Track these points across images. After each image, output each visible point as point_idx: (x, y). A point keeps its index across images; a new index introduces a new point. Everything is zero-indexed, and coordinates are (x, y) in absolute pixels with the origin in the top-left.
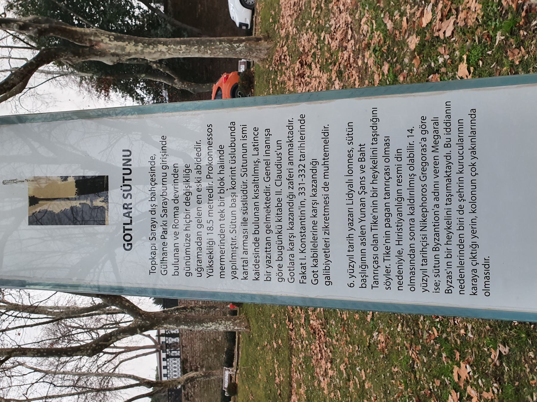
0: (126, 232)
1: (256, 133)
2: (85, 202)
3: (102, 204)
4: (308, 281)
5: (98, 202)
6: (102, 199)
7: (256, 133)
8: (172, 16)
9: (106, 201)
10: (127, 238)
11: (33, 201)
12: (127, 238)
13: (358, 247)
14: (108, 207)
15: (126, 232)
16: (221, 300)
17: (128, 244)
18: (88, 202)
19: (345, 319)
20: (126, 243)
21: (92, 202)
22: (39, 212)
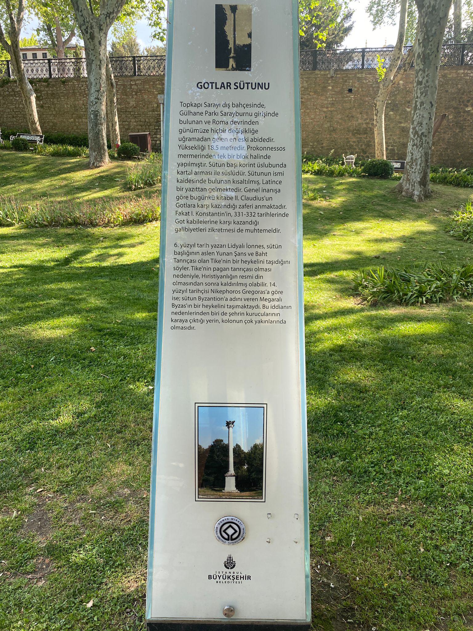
2: (233, 51)
3: (230, 67)
5: (232, 62)
6: (234, 66)
9: (233, 69)
11: (234, 9)
12: (206, 86)
14: (229, 70)
15: (210, 85)
17: (201, 86)
18: (232, 55)
21: (233, 57)
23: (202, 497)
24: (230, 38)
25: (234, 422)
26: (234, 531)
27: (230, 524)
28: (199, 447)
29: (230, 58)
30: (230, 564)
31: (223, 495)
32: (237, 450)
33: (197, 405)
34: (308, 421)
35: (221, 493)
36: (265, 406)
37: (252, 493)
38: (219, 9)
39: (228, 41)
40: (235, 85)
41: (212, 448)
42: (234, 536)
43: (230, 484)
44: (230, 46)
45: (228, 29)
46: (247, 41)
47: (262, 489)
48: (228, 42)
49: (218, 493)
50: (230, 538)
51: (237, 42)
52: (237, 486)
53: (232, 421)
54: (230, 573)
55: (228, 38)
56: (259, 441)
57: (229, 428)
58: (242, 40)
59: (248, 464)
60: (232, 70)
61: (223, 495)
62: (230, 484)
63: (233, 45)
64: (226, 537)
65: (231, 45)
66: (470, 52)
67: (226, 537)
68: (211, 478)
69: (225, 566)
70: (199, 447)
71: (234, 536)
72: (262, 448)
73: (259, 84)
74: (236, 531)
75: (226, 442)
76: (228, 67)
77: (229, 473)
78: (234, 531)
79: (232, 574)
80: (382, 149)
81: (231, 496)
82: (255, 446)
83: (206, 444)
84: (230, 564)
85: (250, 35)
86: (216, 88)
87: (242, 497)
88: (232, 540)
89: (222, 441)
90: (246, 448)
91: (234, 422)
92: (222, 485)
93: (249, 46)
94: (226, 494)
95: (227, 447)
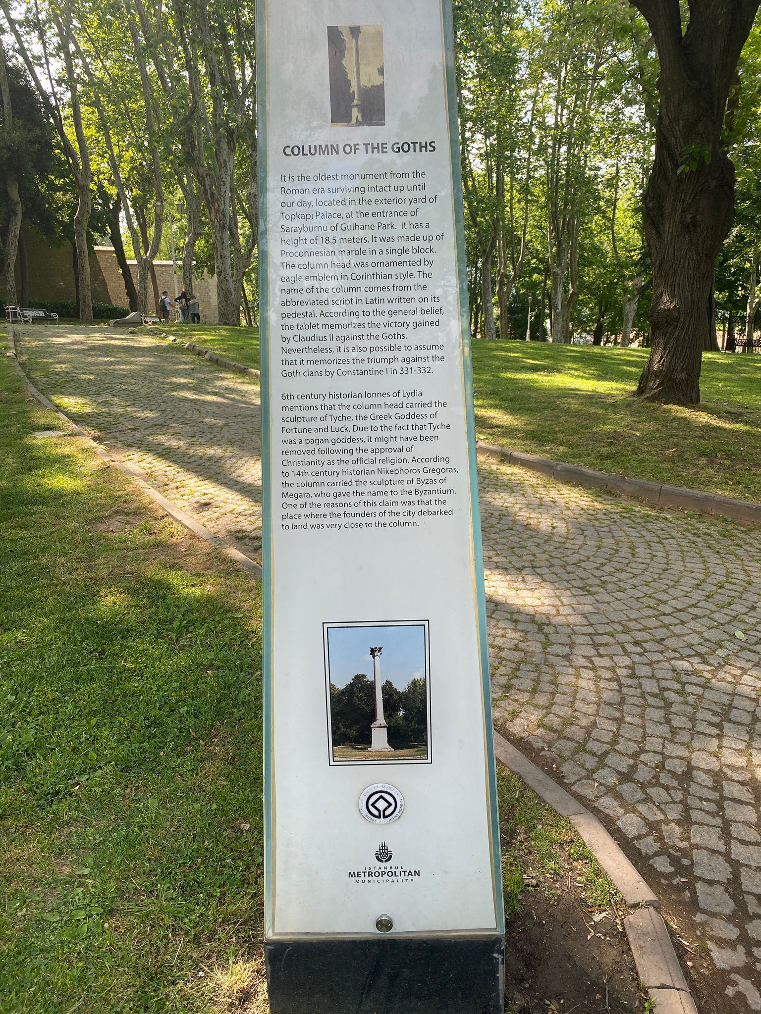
0: (412, 146)
1: (402, 214)
2: (356, 97)
3: (354, 120)
4: (285, 457)
5: (355, 113)
6: (360, 118)
7: (402, 214)
8: (263, 959)
9: (359, 124)
10: (406, 147)
11: (355, 31)
12: (406, 147)
13: (302, 521)
14: (352, 126)
15: (412, 146)
16: (273, 317)
17: (398, 148)
18: (355, 102)
19: (186, 708)
20: (400, 146)
21: (357, 106)
22: (654, 508)
23: (339, 759)
24: (352, 77)
25: (380, 649)
26: (387, 805)
27: (381, 794)
28: (332, 687)
29: (353, 106)
30: (384, 855)
31: (371, 756)
32: (388, 689)
33: (326, 626)
34: (262, 921)
35: (366, 753)
36: (426, 623)
37: (411, 750)
38: (334, 34)
39: (349, 81)
40: (434, 148)
41: (350, 689)
42: (388, 812)
43: (380, 738)
44: (352, 89)
45: (349, 62)
46: (377, 81)
47: (426, 745)
48: (348, 83)
49: (362, 753)
50: (382, 815)
51: (363, 83)
52: (390, 742)
53: (378, 647)
54: (385, 868)
55: (349, 77)
56: (418, 675)
57: (374, 657)
58: (370, 78)
59: (404, 708)
60: (357, 125)
61: (371, 756)
62: (380, 738)
63: (356, 87)
64: (376, 813)
65: (354, 87)
66: (238, 7)
67: (376, 813)
68: (352, 732)
69: (377, 858)
70: (332, 687)
71: (388, 812)
72: (425, 685)
73: (332, 146)
74: (390, 805)
75: (370, 678)
76: (350, 121)
77: (377, 723)
78: (387, 805)
79: (389, 869)
80: (184, 372)
81: (381, 757)
82: (414, 683)
83: (341, 685)
84: (384, 855)
85: (381, 72)
86: (304, 154)
87: (394, 757)
88: (385, 817)
89: (364, 676)
90: (401, 687)
91: (380, 649)
92: (365, 739)
93: (380, 89)
94: (374, 753)
95: (372, 686)
